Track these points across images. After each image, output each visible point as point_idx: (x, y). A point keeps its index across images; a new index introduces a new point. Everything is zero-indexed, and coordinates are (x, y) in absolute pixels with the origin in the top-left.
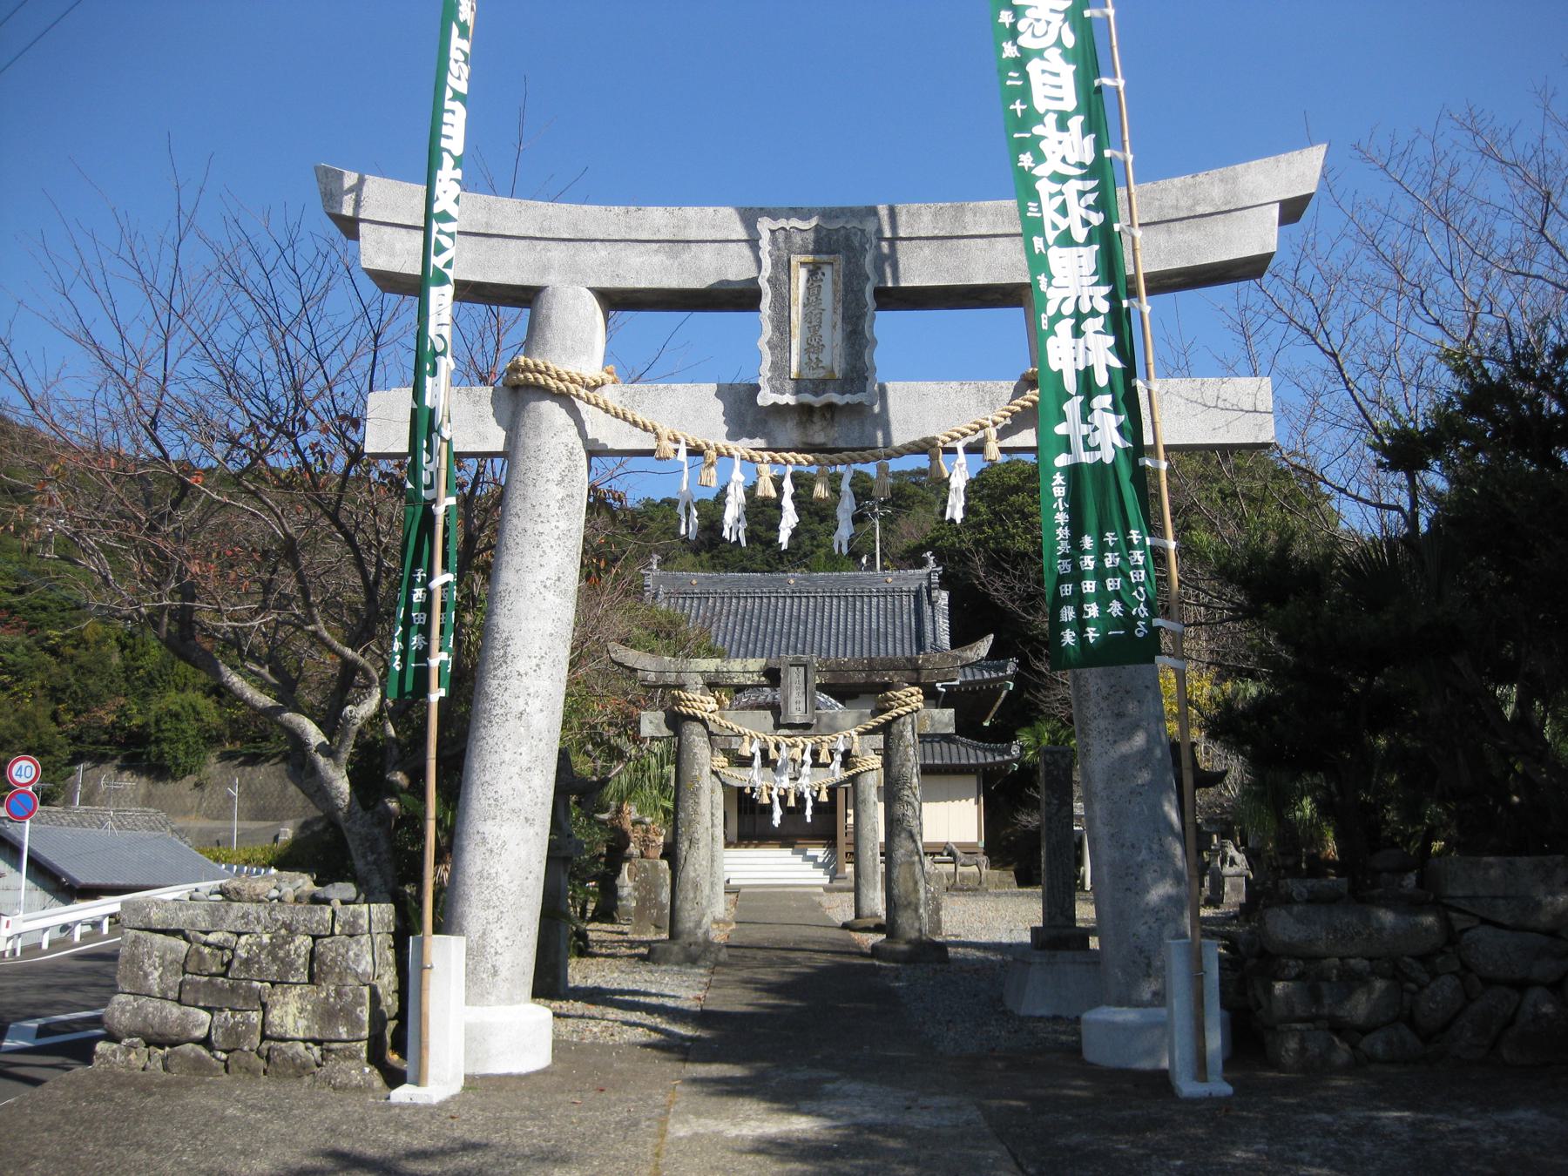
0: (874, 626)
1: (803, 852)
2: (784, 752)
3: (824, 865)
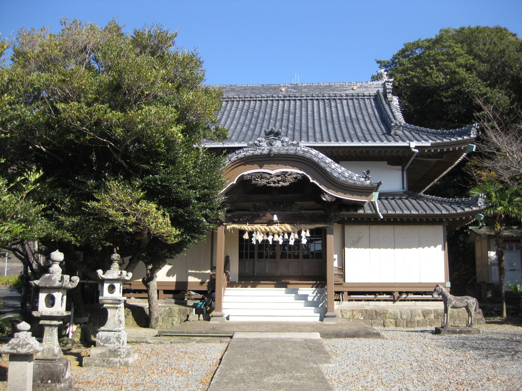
0: (347, 115)
1: (295, 291)
2: (355, 88)
3: (313, 304)
